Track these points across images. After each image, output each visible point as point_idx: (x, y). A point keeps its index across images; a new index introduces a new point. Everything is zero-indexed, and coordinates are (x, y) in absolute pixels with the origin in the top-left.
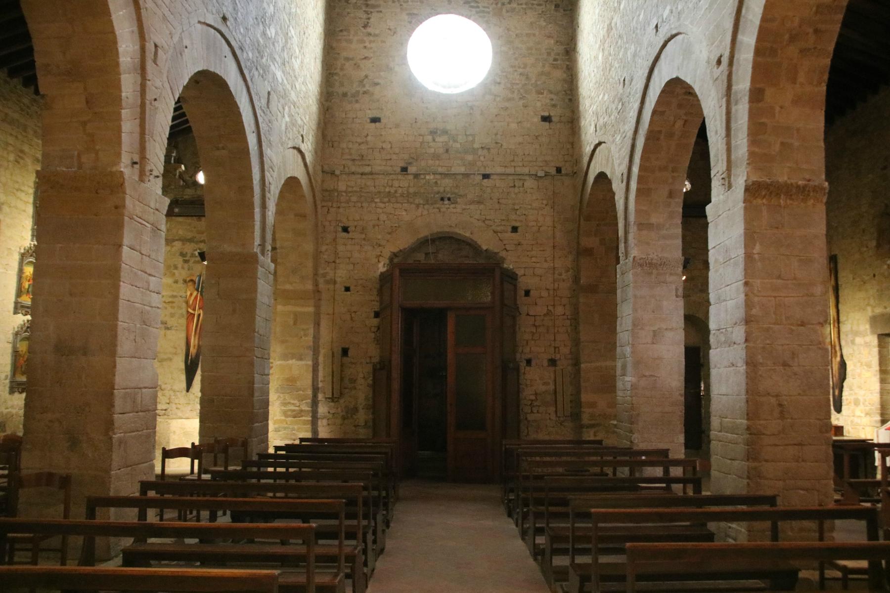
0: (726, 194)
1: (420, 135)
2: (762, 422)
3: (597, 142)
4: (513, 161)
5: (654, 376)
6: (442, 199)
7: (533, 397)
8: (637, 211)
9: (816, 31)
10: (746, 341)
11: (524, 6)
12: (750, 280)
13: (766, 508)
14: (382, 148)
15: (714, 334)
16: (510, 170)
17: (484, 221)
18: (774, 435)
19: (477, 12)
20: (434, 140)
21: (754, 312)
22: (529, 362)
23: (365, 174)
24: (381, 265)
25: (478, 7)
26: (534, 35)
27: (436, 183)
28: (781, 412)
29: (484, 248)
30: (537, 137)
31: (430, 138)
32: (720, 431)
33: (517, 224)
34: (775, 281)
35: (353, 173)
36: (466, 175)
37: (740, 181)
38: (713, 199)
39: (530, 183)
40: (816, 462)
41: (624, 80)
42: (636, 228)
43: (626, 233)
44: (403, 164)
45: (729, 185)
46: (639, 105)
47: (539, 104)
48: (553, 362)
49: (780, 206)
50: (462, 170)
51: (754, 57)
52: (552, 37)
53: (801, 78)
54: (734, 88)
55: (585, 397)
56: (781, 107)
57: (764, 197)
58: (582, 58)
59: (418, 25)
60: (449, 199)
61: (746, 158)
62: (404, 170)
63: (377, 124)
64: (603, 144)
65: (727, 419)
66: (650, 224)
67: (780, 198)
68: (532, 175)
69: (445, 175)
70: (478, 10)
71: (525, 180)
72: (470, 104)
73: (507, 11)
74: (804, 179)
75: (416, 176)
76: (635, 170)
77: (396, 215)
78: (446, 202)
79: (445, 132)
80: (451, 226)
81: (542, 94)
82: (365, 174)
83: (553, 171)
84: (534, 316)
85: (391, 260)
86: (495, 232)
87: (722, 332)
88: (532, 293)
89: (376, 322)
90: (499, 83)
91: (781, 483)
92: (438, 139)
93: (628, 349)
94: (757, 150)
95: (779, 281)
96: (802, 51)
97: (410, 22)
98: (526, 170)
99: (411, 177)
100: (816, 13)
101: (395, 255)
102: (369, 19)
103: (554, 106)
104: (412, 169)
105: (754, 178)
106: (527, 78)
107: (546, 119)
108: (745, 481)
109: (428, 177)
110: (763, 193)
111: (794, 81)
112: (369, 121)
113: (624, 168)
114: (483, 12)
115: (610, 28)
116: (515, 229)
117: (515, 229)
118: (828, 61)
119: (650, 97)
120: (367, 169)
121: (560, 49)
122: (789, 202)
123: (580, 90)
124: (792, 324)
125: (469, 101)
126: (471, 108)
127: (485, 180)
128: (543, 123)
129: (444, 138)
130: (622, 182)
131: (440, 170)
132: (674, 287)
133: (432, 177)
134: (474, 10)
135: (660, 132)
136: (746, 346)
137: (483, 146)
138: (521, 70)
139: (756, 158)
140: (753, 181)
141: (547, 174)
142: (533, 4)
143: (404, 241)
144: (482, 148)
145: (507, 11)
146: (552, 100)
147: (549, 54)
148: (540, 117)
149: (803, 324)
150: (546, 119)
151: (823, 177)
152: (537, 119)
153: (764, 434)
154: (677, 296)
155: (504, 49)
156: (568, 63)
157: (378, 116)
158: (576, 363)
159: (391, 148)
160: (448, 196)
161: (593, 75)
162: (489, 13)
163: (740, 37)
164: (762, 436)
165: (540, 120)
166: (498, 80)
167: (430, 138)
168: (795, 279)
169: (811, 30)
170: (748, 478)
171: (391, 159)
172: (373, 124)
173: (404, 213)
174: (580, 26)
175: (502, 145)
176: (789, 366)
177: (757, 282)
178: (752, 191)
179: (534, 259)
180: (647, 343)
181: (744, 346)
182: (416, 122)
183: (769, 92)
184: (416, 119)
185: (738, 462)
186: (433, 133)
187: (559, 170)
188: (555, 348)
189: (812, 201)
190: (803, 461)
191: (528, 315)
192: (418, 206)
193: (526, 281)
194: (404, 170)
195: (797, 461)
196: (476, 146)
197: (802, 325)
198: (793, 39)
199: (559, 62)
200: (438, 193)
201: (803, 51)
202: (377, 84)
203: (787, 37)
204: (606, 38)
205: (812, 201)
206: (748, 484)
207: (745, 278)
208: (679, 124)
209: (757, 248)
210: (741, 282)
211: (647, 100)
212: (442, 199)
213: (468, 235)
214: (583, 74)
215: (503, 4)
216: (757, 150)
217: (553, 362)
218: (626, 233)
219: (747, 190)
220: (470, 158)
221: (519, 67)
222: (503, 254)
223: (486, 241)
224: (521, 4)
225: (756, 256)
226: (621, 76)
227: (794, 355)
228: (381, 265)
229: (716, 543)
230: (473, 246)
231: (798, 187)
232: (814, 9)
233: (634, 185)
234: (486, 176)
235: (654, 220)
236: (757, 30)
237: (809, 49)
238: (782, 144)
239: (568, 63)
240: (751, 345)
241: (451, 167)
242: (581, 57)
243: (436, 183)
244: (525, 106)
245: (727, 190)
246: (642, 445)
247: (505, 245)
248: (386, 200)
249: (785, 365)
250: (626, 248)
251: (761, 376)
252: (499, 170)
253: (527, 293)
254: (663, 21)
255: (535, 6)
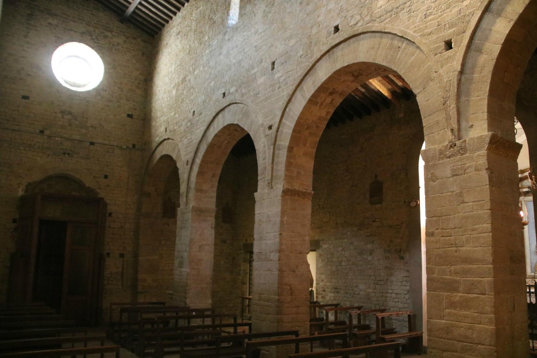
0: (270, 190)
1: (54, 112)
2: (284, 297)
3: (167, 138)
4: (109, 137)
5: (199, 269)
6: (64, 153)
7: (109, 276)
8: (197, 183)
9: (317, 127)
10: (279, 260)
11: (125, 49)
12: (282, 233)
13: (294, 337)
14: (28, 116)
15: (240, 250)
16: (106, 142)
17: (88, 170)
18: (288, 303)
19: (98, 46)
20: (63, 117)
21: (283, 247)
22: (108, 254)
23: (15, 131)
24: (20, 190)
25: (99, 43)
26: (129, 67)
27: (61, 143)
28: (291, 293)
29: (87, 185)
30: (124, 125)
31: (60, 115)
32: (259, 300)
33: (108, 174)
34: (291, 233)
35: (7, 128)
36: (80, 141)
37: (279, 187)
38: (259, 190)
39: (117, 151)
40: (304, 314)
41: (194, 112)
42: (194, 191)
43: (188, 192)
44: (41, 128)
45: (270, 185)
46: (206, 129)
47: (126, 107)
48: (122, 255)
49: (295, 200)
50: (78, 137)
51: (292, 132)
52: (138, 70)
53: (307, 145)
54: (277, 142)
55: (141, 276)
56: (299, 156)
57: (290, 195)
58: (157, 87)
59: (61, 45)
60: (68, 154)
61: (283, 177)
62: (42, 132)
63: (27, 101)
64: (170, 140)
65: (264, 296)
66: (202, 190)
67: (295, 196)
68: (119, 147)
69: (67, 139)
70: (99, 45)
71: (114, 149)
72: (87, 99)
73: (115, 50)
74: (304, 189)
75: (49, 137)
76: (198, 161)
77: (34, 159)
78: (67, 156)
79: (70, 113)
80: (68, 171)
81: (129, 101)
82: (15, 131)
83: (131, 146)
84: (113, 228)
85: (27, 186)
86: (94, 177)
87: (263, 255)
88: (113, 215)
89: (14, 225)
90: (106, 90)
91: (290, 324)
92: (66, 117)
93: (185, 255)
94: (288, 173)
95: (294, 234)
96: (310, 134)
97: (56, 42)
98: (115, 143)
99: (46, 137)
100: (319, 119)
101: (30, 184)
102: (28, 32)
103: (135, 109)
104: (47, 132)
105: (286, 186)
106: (122, 91)
107: (130, 116)
108: (276, 324)
109: (56, 139)
110: (289, 193)
111: (305, 145)
112: (21, 97)
113: (190, 157)
114: (101, 47)
115: (184, 80)
116: (106, 177)
117: (106, 177)
118: (318, 139)
119: (214, 126)
120: (17, 128)
121: (142, 78)
122: (298, 198)
123: (153, 104)
124: (297, 253)
125: (86, 97)
126: (88, 102)
127: (92, 146)
128: (128, 118)
129: (69, 117)
130: (187, 164)
131: (65, 136)
132: (210, 223)
133: (59, 139)
134: (96, 44)
135: (215, 145)
136: (279, 263)
137: (92, 125)
138: (119, 85)
139: (288, 178)
140: (286, 188)
141: (127, 147)
142: (130, 49)
143: (37, 176)
144: (91, 126)
145: (115, 50)
146: (134, 105)
147: (136, 80)
148: (126, 114)
149: (301, 253)
150: (130, 116)
151: (311, 189)
152: (125, 115)
153: (284, 303)
154: (212, 228)
155: (111, 71)
156: (145, 87)
157: (28, 95)
158: (136, 256)
159: (35, 117)
160: (68, 152)
161: (166, 100)
162: (104, 48)
163: (284, 120)
164: (284, 303)
165: (126, 116)
166: (105, 88)
167: (60, 115)
168: (299, 233)
169: (315, 126)
170: (278, 322)
171: (33, 124)
172: (24, 100)
173: (39, 159)
174: (157, 69)
175: (103, 127)
176: (295, 272)
177: (284, 234)
178: (286, 192)
179: (116, 195)
180: (196, 252)
181: (278, 262)
182: (52, 104)
183: (295, 149)
184: (52, 102)
185: (272, 315)
186: (63, 112)
187: (134, 146)
188: (123, 247)
189: (307, 199)
190: (299, 314)
191: (110, 227)
192: (49, 155)
193: (111, 208)
194: (42, 132)
195: (297, 314)
196: (88, 125)
197: (300, 254)
198: (308, 127)
199: (140, 85)
200: (62, 149)
201: (310, 134)
202: (29, 75)
203: (306, 127)
204: (180, 84)
205: (307, 199)
206: (278, 325)
207: (280, 231)
208: (226, 142)
209: (285, 219)
210: (278, 233)
211: (211, 129)
212: (64, 153)
213: (78, 176)
214: (157, 97)
215: (114, 45)
216: (288, 173)
217: (122, 255)
218: (188, 192)
219: (283, 191)
220: (84, 131)
221: (118, 84)
222: (98, 191)
223: (88, 182)
224: (123, 48)
225: (285, 222)
226: (192, 109)
227: (297, 267)
228: (20, 190)
229: (300, 354)
230: (80, 185)
231: (303, 192)
232: (318, 118)
233: (196, 169)
234: (92, 144)
235: (204, 187)
236: (295, 122)
237: (313, 133)
238: (298, 172)
239: (145, 87)
240: (281, 262)
241: (72, 135)
242: (158, 89)
243: (61, 143)
244: (119, 106)
245: (270, 188)
246: (192, 306)
247: (99, 185)
248: (27, 149)
249: (294, 271)
250: (187, 200)
251: (284, 276)
252: (100, 141)
253: (110, 215)
254: (229, 93)
255: (132, 51)
